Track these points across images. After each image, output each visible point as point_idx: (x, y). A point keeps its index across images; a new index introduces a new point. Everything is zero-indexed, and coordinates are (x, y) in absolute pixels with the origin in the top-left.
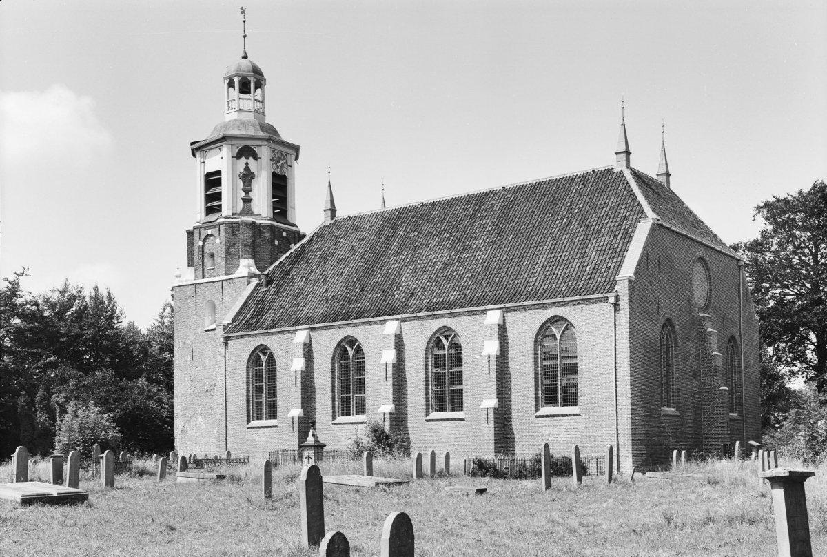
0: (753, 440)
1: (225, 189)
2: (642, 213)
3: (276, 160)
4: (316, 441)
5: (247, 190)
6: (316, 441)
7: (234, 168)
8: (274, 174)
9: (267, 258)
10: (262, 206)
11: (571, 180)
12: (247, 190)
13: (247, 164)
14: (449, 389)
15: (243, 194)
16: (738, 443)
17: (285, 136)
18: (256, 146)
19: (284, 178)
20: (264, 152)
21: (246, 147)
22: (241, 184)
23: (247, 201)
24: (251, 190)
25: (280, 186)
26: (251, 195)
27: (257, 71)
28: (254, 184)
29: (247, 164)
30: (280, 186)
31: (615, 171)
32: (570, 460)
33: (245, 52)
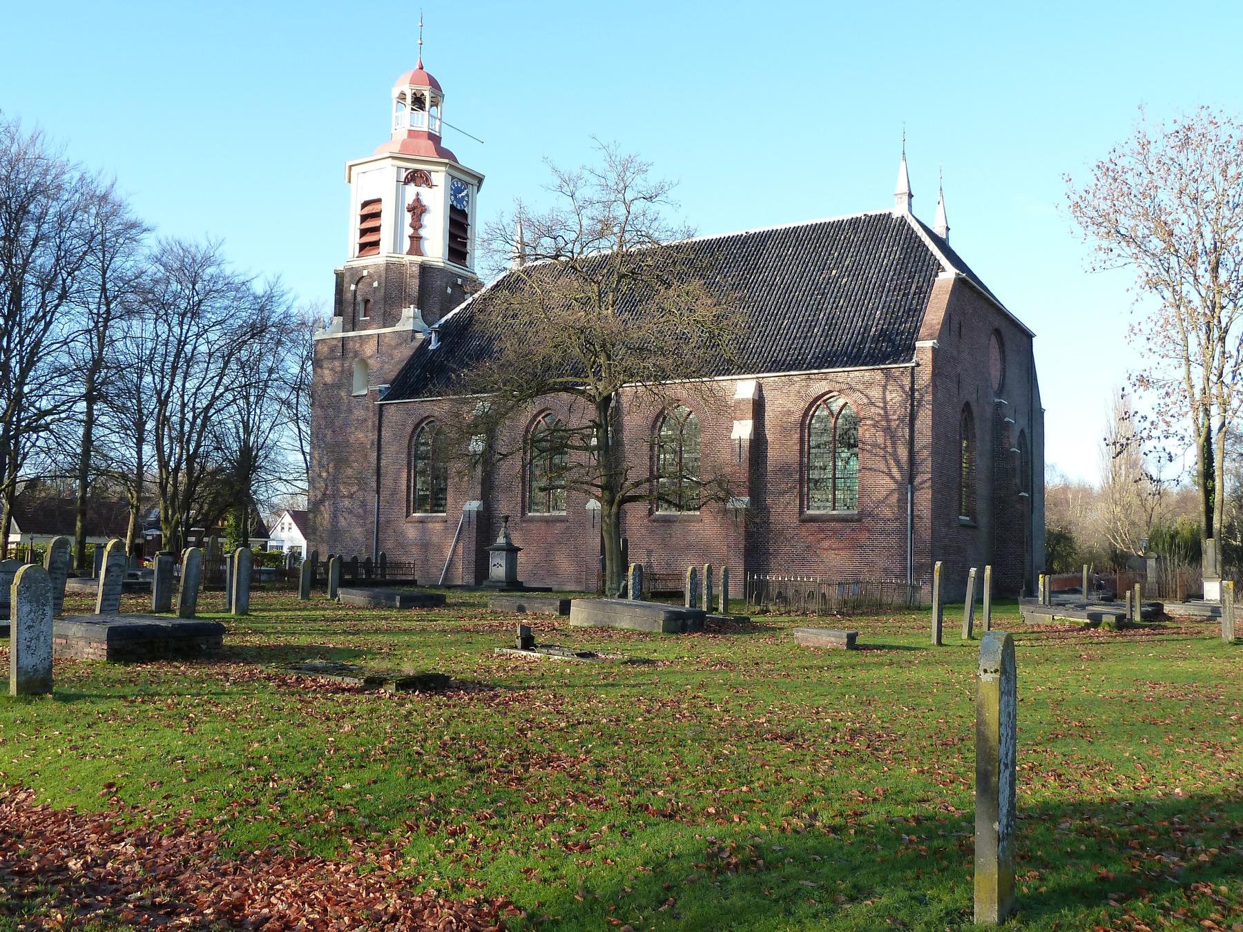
0: (993, 571)
1: (386, 222)
2: (940, 267)
3: (456, 191)
4: (509, 544)
6: (509, 544)
7: (399, 196)
8: (452, 207)
9: (436, 310)
10: (435, 250)
11: (840, 224)
14: (132, 541)
15: (411, 231)
16: (938, 564)
17: (465, 161)
19: (464, 214)
20: (439, 177)
21: (416, 171)
22: (408, 217)
23: (416, 239)
24: (421, 226)
25: (459, 224)
26: (422, 232)
28: (426, 219)
30: (459, 224)
31: (894, 216)
32: (482, 285)
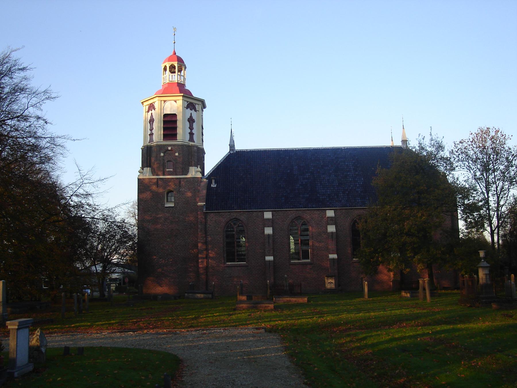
5: (191, 128)
12: (191, 128)
13: (191, 114)
18: (196, 104)
23: (191, 134)
27: (180, 60)
29: (191, 114)
33: (404, 135)
